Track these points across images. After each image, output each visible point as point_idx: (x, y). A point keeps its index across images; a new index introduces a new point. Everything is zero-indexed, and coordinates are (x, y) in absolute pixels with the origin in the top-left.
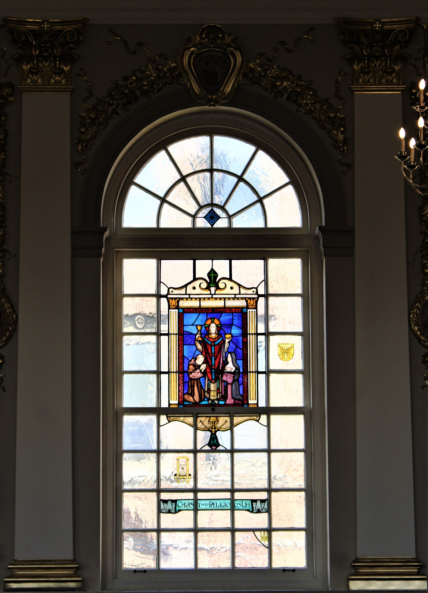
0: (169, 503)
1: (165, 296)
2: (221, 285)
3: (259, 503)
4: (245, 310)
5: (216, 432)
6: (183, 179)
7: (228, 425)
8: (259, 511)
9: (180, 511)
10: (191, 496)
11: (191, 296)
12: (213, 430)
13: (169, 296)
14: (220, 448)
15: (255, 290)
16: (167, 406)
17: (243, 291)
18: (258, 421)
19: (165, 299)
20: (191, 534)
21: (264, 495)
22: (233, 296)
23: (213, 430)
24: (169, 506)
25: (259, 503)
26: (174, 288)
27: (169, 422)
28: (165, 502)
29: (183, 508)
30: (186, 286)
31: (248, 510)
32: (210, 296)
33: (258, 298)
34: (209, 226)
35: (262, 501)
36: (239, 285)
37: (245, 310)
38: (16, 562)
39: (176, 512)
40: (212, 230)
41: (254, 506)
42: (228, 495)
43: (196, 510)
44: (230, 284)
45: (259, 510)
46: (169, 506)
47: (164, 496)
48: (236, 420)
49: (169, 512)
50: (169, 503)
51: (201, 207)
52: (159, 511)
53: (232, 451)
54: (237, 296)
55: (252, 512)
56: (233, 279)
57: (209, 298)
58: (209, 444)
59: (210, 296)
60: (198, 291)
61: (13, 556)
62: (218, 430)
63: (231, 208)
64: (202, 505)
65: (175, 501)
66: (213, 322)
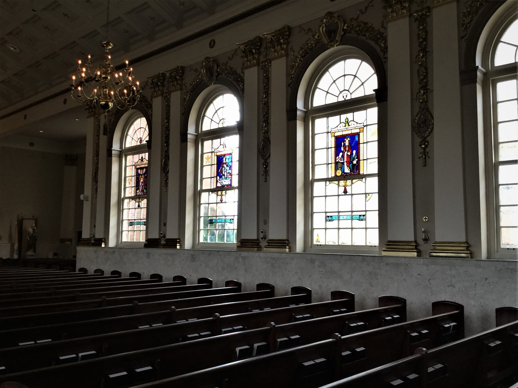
0: (330, 217)
1: (330, 132)
2: (350, 124)
3: (362, 216)
4: (359, 133)
5: (346, 186)
6: (355, 76)
7: (350, 183)
8: (362, 220)
9: (333, 220)
10: (337, 214)
11: (339, 131)
12: (345, 186)
13: (215, 152)
14: (347, 193)
15: (363, 124)
16: (331, 177)
17: (358, 125)
18: (362, 181)
19: (330, 133)
20: (337, 230)
21: (364, 213)
22: (355, 128)
23: (345, 186)
24: (330, 218)
25: (362, 216)
26: (216, 149)
27: (330, 184)
28: (328, 217)
29: (334, 219)
30: (137, 162)
31: (358, 220)
32: (346, 129)
33: (364, 127)
34: (140, 144)
35: (364, 216)
36: (357, 123)
37: (359, 133)
38: (436, 243)
39: (332, 221)
40: (141, 145)
41: (360, 218)
42: (350, 213)
43: (339, 220)
44: (353, 123)
45: (362, 219)
46: (330, 218)
47: (328, 214)
48: (354, 181)
49: (330, 221)
50: (330, 217)
51: (139, 139)
52: (326, 221)
53: (352, 195)
54: (356, 128)
55: (360, 220)
56: (354, 121)
57: (345, 130)
58: (344, 192)
59: (346, 129)
60: (342, 128)
61: (435, 239)
62: (347, 186)
63: (351, 91)
64: (341, 218)
65: (331, 216)
66: (347, 139)
